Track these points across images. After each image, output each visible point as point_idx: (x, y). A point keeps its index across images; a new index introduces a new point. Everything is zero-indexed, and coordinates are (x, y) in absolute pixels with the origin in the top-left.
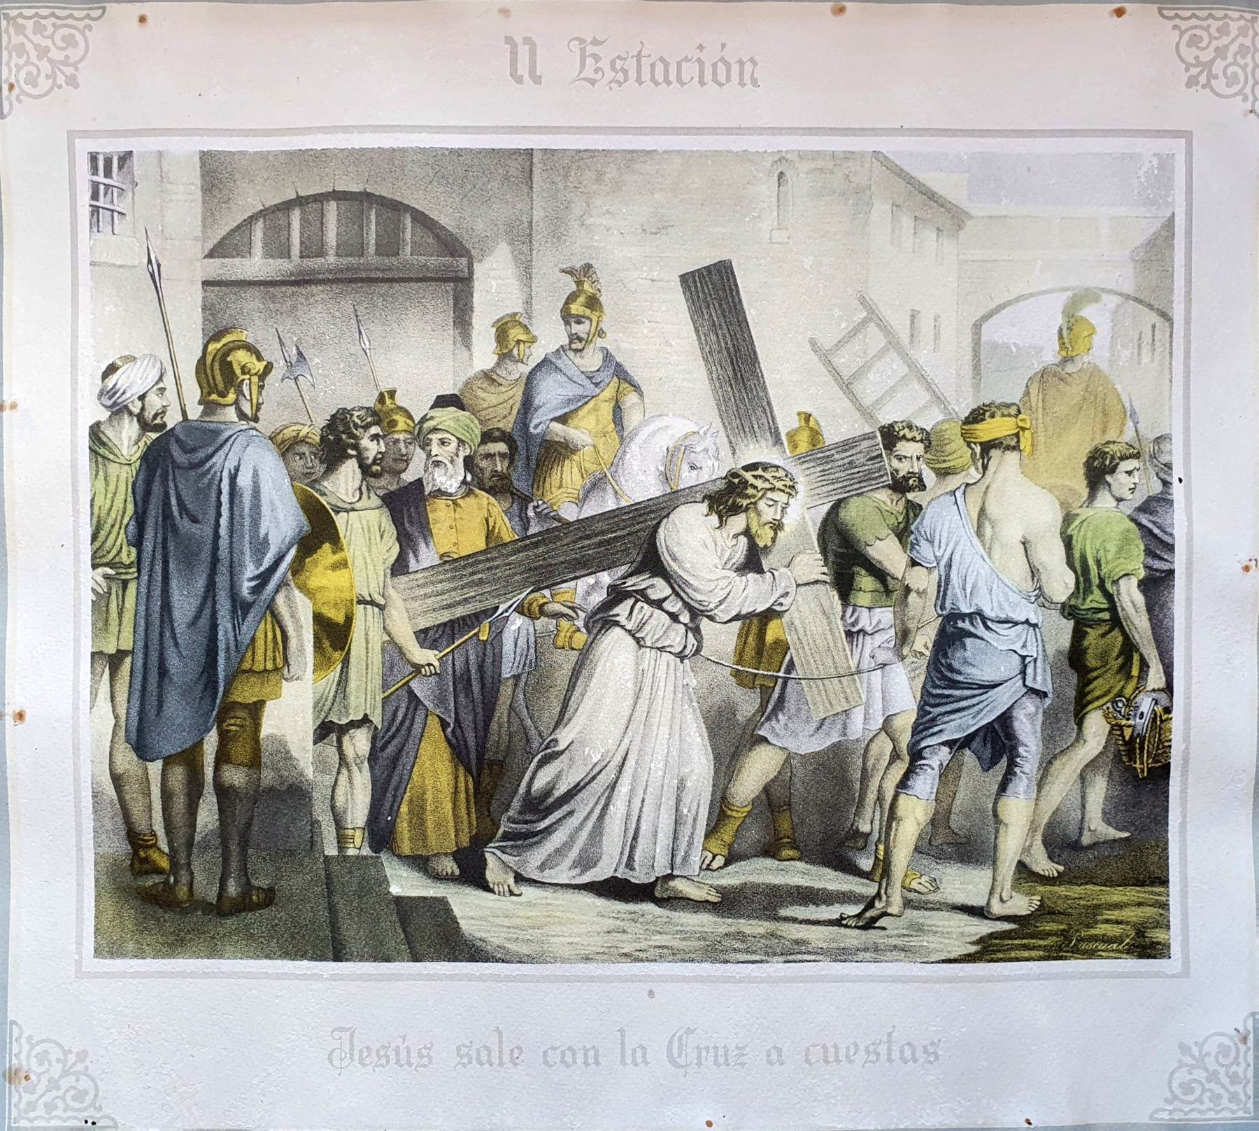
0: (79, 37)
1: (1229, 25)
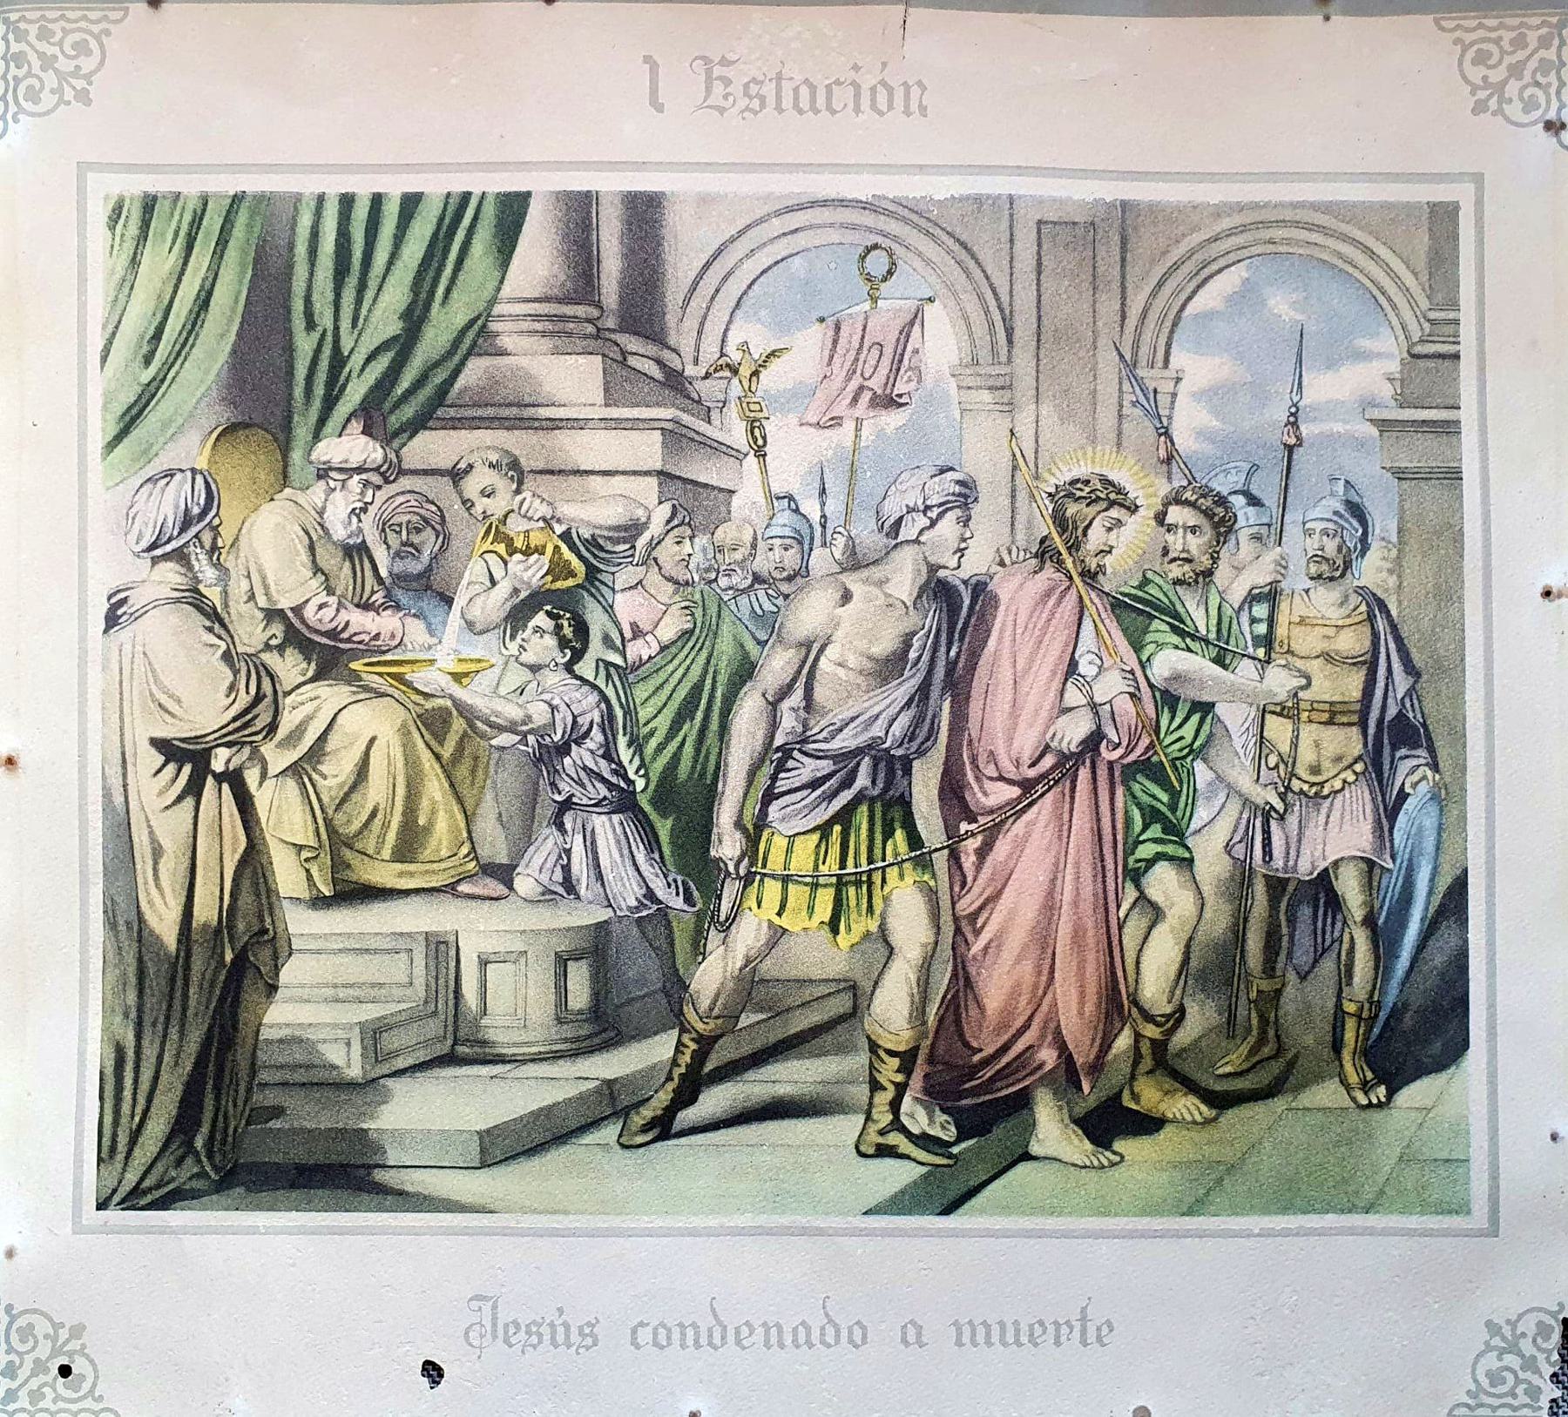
0: (93, 44)
1: (1526, 35)
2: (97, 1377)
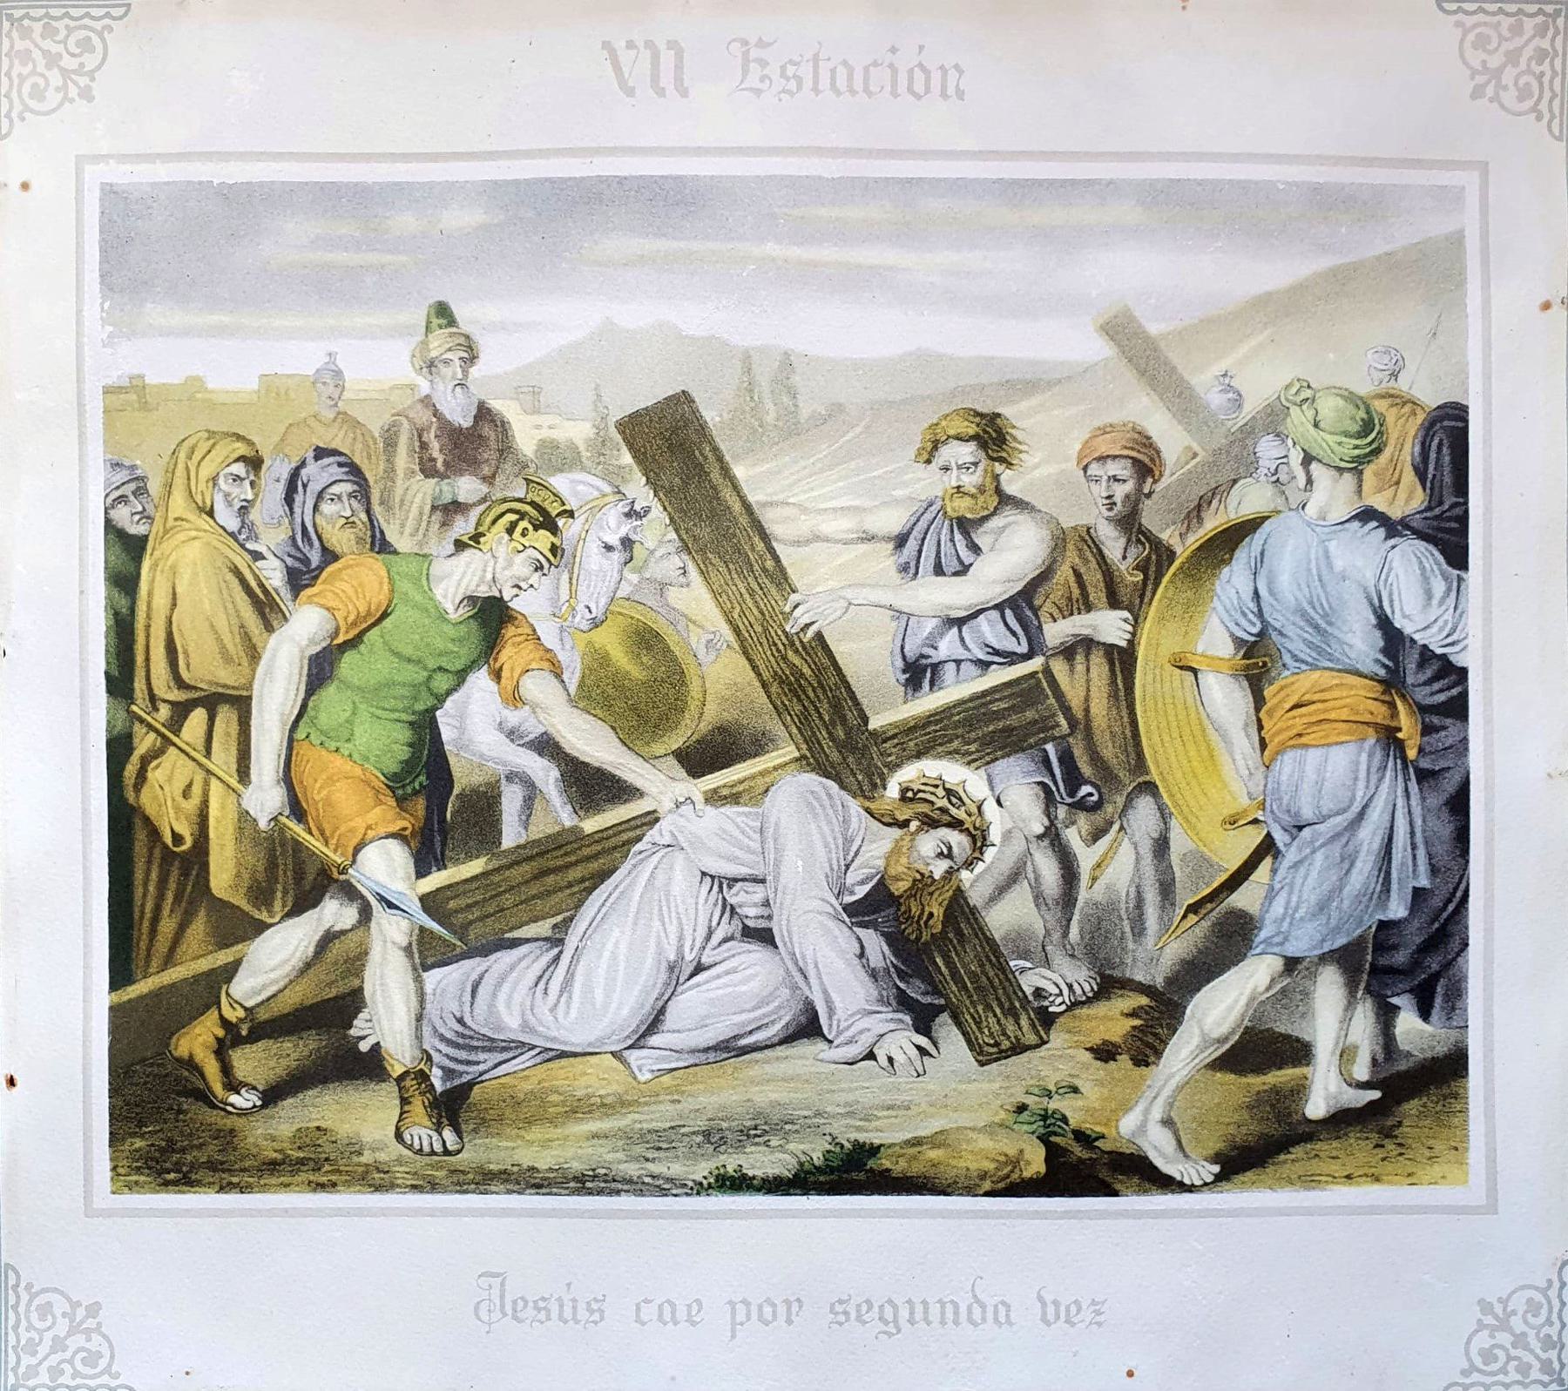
2: (112, 1357)
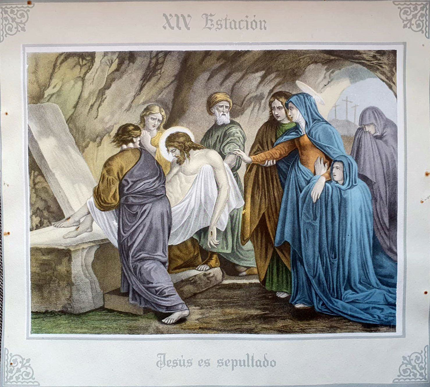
0: (25, 14)
2: (33, 371)
